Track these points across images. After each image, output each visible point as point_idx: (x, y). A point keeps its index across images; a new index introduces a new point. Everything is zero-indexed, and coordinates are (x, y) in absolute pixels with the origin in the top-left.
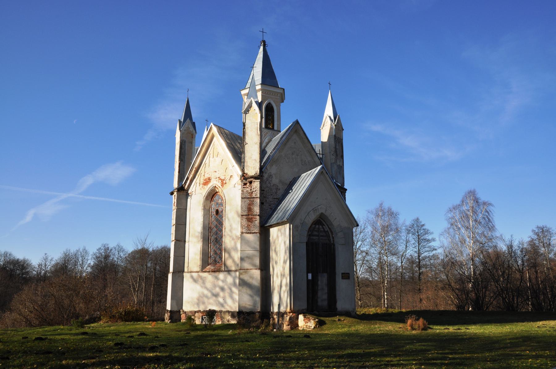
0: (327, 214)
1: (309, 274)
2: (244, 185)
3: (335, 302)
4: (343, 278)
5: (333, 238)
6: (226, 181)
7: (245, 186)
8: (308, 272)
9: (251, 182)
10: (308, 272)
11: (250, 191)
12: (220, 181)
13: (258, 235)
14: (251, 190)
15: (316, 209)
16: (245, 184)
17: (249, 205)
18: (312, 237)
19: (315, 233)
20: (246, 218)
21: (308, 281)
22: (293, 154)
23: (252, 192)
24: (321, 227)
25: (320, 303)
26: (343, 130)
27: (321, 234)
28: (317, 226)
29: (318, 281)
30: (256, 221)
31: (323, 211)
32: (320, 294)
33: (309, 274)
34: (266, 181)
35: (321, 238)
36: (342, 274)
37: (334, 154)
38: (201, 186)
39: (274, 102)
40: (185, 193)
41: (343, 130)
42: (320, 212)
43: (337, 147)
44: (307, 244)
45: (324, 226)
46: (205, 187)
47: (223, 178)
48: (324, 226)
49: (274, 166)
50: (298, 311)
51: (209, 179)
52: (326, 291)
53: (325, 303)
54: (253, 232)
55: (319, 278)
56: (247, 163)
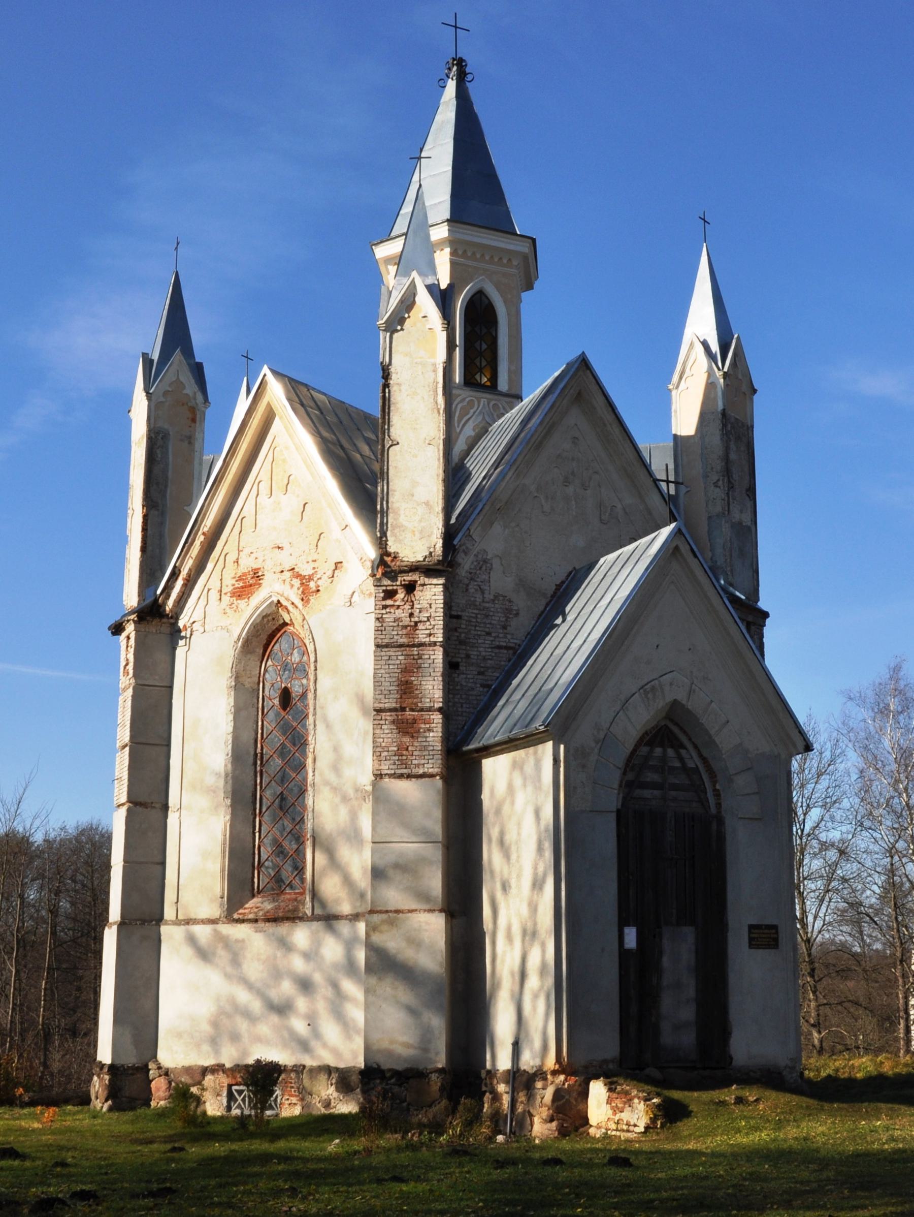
0: (695, 705)
1: (627, 930)
2: (384, 599)
3: (725, 1033)
4: (754, 943)
5: (717, 794)
6: (320, 583)
7: (389, 602)
8: (622, 923)
9: (410, 588)
10: (622, 923)
11: (406, 621)
12: (297, 582)
13: (438, 782)
14: (411, 615)
15: (653, 689)
16: (390, 594)
17: (406, 670)
18: (638, 792)
19: (651, 777)
20: (393, 722)
21: (624, 954)
22: (566, 482)
23: (416, 623)
24: (671, 752)
25: (667, 1038)
26: (755, 391)
27: (673, 780)
28: (658, 751)
29: (661, 953)
30: (429, 730)
31: (681, 696)
32: (667, 1002)
33: (627, 930)
34: (466, 581)
35: (673, 793)
36: (751, 927)
37: (720, 483)
38: (226, 599)
39: (497, 287)
40: (166, 629)
41: (755, 391)
42: (669, 698)
43: (733, 456)
44: (620, 815)
45: (683, 752)
46: (242, 603)
47: (306, 571)
48: (683, 752)
49: (497, 528)
50: (586, 1067)
51: (257, 575)
52: (691, 991)
53: (688, 1039)
54: (421, 771)
55: (666, 944)
56: (396, 513)
